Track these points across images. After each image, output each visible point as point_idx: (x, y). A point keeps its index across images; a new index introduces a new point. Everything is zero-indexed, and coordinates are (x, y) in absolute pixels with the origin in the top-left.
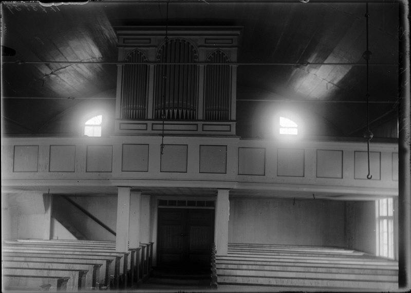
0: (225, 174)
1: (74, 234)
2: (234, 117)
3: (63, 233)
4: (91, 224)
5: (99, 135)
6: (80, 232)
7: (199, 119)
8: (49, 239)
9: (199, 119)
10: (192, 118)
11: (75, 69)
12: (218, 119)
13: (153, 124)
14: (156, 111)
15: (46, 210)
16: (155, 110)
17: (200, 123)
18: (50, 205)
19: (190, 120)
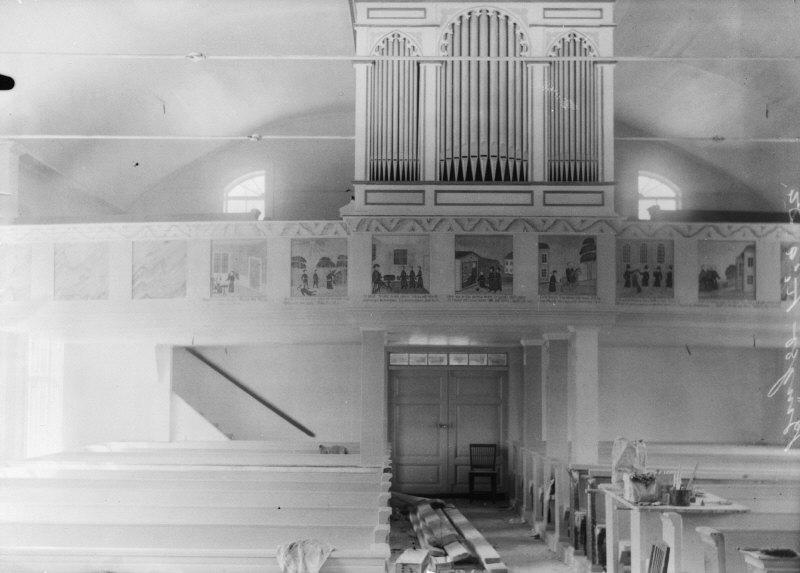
14: (443, 163)
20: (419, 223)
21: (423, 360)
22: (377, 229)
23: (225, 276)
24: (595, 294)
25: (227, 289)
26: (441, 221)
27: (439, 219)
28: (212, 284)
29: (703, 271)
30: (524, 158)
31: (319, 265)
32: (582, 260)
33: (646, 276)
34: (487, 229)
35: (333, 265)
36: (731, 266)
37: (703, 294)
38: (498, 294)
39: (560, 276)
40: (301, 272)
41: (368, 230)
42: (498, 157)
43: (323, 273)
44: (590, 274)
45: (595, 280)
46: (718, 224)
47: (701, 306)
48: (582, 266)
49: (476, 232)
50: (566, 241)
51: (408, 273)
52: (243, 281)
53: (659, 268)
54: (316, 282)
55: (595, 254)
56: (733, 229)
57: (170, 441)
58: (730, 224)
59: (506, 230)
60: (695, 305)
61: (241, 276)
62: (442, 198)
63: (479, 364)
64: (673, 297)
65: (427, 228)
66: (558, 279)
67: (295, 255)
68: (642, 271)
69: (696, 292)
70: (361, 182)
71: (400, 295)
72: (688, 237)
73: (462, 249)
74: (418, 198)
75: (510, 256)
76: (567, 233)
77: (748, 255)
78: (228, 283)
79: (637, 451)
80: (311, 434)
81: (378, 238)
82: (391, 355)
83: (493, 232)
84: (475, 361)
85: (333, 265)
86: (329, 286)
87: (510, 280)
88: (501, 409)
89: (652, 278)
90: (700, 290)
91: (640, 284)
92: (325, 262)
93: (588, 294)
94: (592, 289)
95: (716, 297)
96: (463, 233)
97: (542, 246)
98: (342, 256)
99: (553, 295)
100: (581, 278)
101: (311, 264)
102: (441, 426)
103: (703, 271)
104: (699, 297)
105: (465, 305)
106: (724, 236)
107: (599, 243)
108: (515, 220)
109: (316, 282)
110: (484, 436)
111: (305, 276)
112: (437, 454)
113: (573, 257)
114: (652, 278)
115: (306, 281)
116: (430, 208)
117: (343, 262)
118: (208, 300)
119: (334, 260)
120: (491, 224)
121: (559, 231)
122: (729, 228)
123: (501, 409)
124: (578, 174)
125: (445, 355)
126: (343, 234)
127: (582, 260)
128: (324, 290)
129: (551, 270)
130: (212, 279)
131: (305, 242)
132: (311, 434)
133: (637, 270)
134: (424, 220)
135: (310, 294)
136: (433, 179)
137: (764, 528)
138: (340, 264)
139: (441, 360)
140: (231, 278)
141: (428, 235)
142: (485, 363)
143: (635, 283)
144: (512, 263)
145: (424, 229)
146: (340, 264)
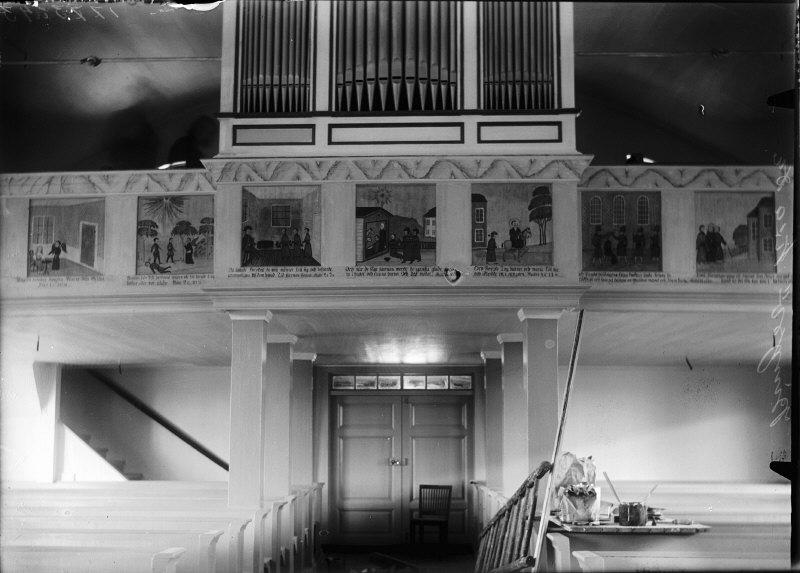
0: (327, 141)
1: (120, 466)
2: (569, 99)
3: (87, 465)
4: (162, 438)
5: (368, 349)
6: (134, 465)
7: (466, 107)
8: (51, 481)
9: (466, 107)
10: (445, 105)
11: (625, 238)
12: (530, 106)
13: (331, 127)
14: (340, 90)
15: (43, 403)
16: (337, 85)
17: (471, 122)
18: (55, 387)
19: (439, 112)
20: (306, 168)
21: (372, 384)
22: (249, 177)
23: (47, 248)
24: (552, 264)
25: (50, 266)
26: (336, 165)
27: (332, 161)
28: (30, 259)
29: (702, 233)
30: (452, 80)
31: (175, 232)
32: (532, 218)
33: (623, 241)
34: (400, 176)
35: (194, 231)
36: (740, 227)
37: (703, 266)
38: (416, 265)
39: (502, 239)
40: (150, 241)
41: (235, 179)
42: (416, 79)
43: (179, 243)
44: (543, 236)
45: (552, 243)
46: (719, 168)
47: (702, 281)
48: (533, 225)
49: (385, 180)
50: (510, 191)
51: (291, 238)
52: (73, 254)
53: (641, 229)
54: (170, 255)
55: (550, 208)
56: (744, 174)
57: (55, 481)
58: (738, 168)
59: (427, 176)
60: (692, 281)
61: (68, 248)
62: (339, 134)
63: (438, 387)
64: (660, 269)
65: (316, 173)
66: (499, 244)
67: (144, 218)
68: (617, 234)
69: (692, 261)
70: (227, 115)
71: (279, 268)
72: (681, 186)
73: (365, 204)
74: (306, 134)
75: (432, 213)
76: (511, 180)
77: (764, 212)
78: (52, 256)
79: (586, 470)
80: (226, 467)
81: (250, 190)
82: (334, 377)
83: (406, 180)
84: (434, 384)
85: (194, 231)
86: (189, 260)
87: (432, 245)
88: (465, 441)
89: (631, 244)
90: (699, 260)
91: (615, 253)
92: (183, 228)
93: (540, 264)
94: (548, 259)
95: (721, 270)
96: (365, 181)
97: (478, 199)
98: (207, 219)
99: (491, 265)
100: (530, 242)
101: (164, 232)
102: (394, 463)
103: (702, 233)
104: (698, 271)
105: (367, 281)
106: (730, 186)
107: (556, 191)
108: (437, 163)
109: (170, 255)
110: (448, 479)
111: (156, 246)
112: (390, 498)
113: (520, 212)
114: (631, 244)
115: (157, 255)
116: (322, 147)
117: (208, 226)
118: (23, 281)
119: (196, 225)
120: (405, 168)
121: (498, 177)
122: (737, 172)
123: (465, 441)
124: (533, 98)
125: (397, 378)
126: (207, 189)
127: (532, 218)
128: (182, 265)
129: (489, 232)
130: (30, 253)
131: (156, 201)
132: (226, 467)
133: (612, 234)
134: (313, 166)
135: (163, 271)
136: (327, 109)
137: (223, 69)
138: (203, 230)
139: (394, 384)
140: (56, 251)
141: (319, 186)
142: (446, 387)
143: (608, 251)
144: (434, 223)
145: (313, 177)
146: (203, 230)
